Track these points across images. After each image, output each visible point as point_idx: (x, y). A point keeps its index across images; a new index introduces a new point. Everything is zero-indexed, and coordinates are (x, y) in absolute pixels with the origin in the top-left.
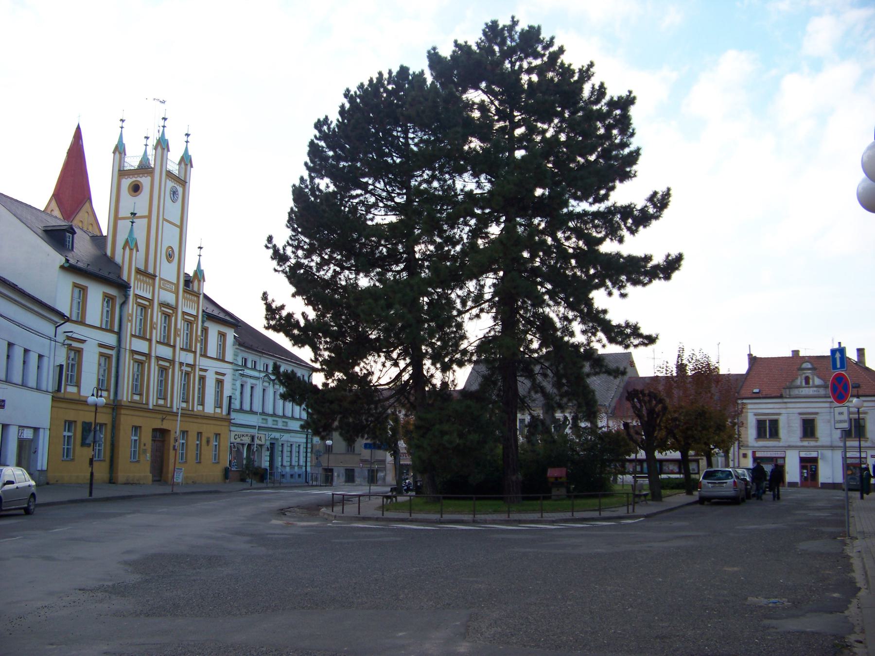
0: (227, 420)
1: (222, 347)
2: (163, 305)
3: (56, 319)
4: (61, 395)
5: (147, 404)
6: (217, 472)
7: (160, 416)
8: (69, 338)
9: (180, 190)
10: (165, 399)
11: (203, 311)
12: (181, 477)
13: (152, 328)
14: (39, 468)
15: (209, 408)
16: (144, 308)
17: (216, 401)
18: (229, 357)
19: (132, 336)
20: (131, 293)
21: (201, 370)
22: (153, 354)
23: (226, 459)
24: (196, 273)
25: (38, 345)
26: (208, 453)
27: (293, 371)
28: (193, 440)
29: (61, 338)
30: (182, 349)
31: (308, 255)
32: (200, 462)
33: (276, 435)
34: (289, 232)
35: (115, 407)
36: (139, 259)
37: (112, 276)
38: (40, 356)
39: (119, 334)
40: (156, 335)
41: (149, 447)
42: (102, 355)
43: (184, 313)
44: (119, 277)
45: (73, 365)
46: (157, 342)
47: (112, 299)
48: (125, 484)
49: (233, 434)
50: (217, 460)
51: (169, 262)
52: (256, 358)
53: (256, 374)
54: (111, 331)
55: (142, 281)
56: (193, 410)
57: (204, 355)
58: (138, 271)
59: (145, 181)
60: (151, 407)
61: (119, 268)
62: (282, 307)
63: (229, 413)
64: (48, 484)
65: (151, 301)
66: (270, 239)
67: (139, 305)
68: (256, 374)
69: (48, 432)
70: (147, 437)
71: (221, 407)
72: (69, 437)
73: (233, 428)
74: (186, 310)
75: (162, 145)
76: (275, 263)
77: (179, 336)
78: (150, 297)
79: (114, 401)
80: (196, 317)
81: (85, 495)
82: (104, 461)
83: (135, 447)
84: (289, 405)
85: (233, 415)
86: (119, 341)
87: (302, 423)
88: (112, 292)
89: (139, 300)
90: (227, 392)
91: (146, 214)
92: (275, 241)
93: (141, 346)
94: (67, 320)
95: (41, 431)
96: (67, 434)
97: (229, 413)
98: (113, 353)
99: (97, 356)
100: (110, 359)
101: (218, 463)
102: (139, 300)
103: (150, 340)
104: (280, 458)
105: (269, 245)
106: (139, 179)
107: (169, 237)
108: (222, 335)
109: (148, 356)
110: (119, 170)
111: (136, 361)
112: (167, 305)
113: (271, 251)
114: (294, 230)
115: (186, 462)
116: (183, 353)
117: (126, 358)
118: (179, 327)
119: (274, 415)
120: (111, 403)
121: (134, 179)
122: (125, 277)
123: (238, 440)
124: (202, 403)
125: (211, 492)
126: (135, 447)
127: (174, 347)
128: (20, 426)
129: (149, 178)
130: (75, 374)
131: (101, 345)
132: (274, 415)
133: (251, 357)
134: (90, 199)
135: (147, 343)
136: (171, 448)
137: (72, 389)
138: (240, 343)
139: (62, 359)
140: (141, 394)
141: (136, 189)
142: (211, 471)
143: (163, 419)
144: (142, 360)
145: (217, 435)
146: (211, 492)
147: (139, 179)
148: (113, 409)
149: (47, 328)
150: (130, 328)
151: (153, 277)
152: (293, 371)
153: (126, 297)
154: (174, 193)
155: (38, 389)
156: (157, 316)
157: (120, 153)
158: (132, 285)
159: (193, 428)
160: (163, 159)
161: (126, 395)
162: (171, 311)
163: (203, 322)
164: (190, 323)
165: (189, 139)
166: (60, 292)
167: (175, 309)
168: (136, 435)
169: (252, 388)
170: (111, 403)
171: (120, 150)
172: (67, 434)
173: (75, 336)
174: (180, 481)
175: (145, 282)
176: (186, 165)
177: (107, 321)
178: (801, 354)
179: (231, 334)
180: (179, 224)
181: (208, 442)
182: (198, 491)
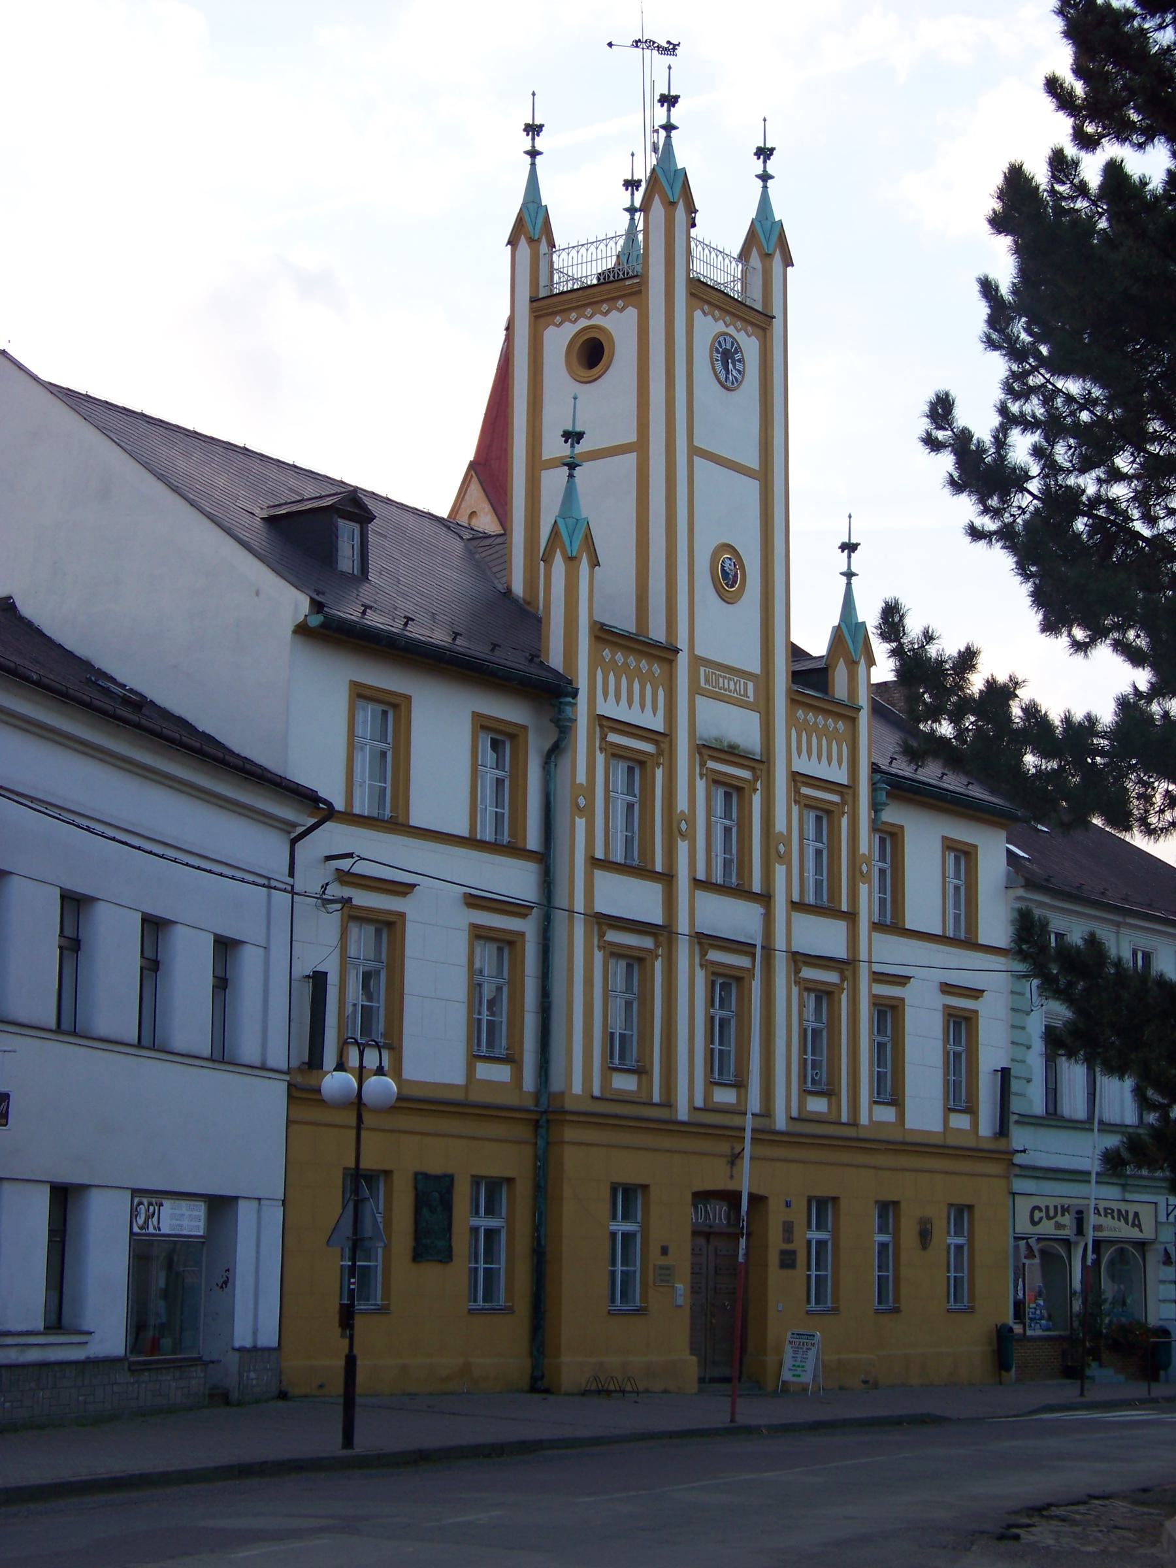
0: (999, 1155)
2: (707, 750)
3: (287, 812)
5: (668, 1103)
6: (967, 1343)
8: (344, 877)
9: (749, 346)
10: (830, 1093)
11: (875, 769)
12: (810, 1366)
13: (672, 835)
14: (242, 1337)
15: (924, 1110)
16: (637, 764)
21: (879, 977)
22: (683, 926)
25: (244, 912)
26: (924, 1276)
27: (1092, 941)
28: (860, 1233)
29: (311, 877)
30: (797, 906)
31: (1096, 450)
32: (896, 1310)
34: (998, 366)
35: (544, 1118)
36: (609, 592)
37: (510, 658)
38: (225, 947)
39: (544, 859)
41: (682, 1257)
42: (479, 934)
43: (797, 778)
44: (536, 656)
45: (723, 1023)
46: (594, 863)
47: (512, 737)
48: (584, 1393)
49: (1023, 1206)
50: (961, 1293)
51: (728, 599)
54: (514, 849)
55: (810, 730)
56: (854, 1124)
57: (891, 923)
58: (604, 635)
59: (619, 325)
60: (683, 1114)
62: (967, 659)
63: (1003, 1131)
64: (283, 1396)
66: (941, 409)
67: (616, 754)
69: (274, 1215)
70: (671, 1223)
71: (970, 1109)
72: (821, 1244)
73: (1020, 1185)
74: (803, 765)
75: (665, 191)
76: (966, 508)
77: (785, 859)
78: (657, 723)
79: (537, 1096)
80: (847, 790)
81: (329, 1442)
82: (509, 1310)
83: (490, 1254)
84: (1074, 1074)
85: (1020, 1137)
86: (547, 883)
87: (1112, 1141)
88: (508, 710)
90: (992, 1051)
91: (633, 438)
92: (963, 417)
93: (636, 899)
95: (245, 1213)
96: (621, 1227)
97: (1003, 1131)
98: (527, 927)
99: (460, 942)
100: (514, 950)
101: (971, 1310)
102: (613, 738)
103: (667, 878)
105: (941, 435)
106: (598, 320)
107: (721, 511)
109: (663, 933)
110: (534, 300)
111: (808, 987)
112: (732, 753)
113: (946, 462)
114: (1015, 353)
115: (835, 1310)
117: (576, 940)
118: (780, 825)
120: (529, 1103)
121: (583, 323)
122: (556, 660)
123: (1047, 1228)
124: (891, 1091)
125: (896, 1422)
126: (490, 1254)
127: (765, 898)
128: (135, 1192)
129: (632, 313)
130: (380, 1004)
131: (474, 901)
135: (757, 910)
136: (773, 1258)
140: (642, 1071)
142: (941, 1340)
144: (638, 951)
145: (962, 1212)
146: (896, 1422)
147: (598, 320)
148: (536, 1125)
149: (263, 849)
150: (577, 840)
152: (1092, 941)
153: (563, 728)
154: (727, 356)
155: (222, 1055)
156: (690, 791)
157: (533, 241)
158: (582, 684)
159: (858, 1187)
161: (580, 1073)
162: (746, 774)
163: (876, 807)
164: (825, 814)
166: (306, 719)
167: (761, 764)
168: (959, 1233)
170: (529, 1103)
171: (532, 229)
172: (621, 1227)
173: (361, 868)
174: (807, 1378)
175: (823, 733)
176: (767, 257)
177: (957, 917)
180: (754, 463)
181: (925, 1235)
182: (882, 1417)
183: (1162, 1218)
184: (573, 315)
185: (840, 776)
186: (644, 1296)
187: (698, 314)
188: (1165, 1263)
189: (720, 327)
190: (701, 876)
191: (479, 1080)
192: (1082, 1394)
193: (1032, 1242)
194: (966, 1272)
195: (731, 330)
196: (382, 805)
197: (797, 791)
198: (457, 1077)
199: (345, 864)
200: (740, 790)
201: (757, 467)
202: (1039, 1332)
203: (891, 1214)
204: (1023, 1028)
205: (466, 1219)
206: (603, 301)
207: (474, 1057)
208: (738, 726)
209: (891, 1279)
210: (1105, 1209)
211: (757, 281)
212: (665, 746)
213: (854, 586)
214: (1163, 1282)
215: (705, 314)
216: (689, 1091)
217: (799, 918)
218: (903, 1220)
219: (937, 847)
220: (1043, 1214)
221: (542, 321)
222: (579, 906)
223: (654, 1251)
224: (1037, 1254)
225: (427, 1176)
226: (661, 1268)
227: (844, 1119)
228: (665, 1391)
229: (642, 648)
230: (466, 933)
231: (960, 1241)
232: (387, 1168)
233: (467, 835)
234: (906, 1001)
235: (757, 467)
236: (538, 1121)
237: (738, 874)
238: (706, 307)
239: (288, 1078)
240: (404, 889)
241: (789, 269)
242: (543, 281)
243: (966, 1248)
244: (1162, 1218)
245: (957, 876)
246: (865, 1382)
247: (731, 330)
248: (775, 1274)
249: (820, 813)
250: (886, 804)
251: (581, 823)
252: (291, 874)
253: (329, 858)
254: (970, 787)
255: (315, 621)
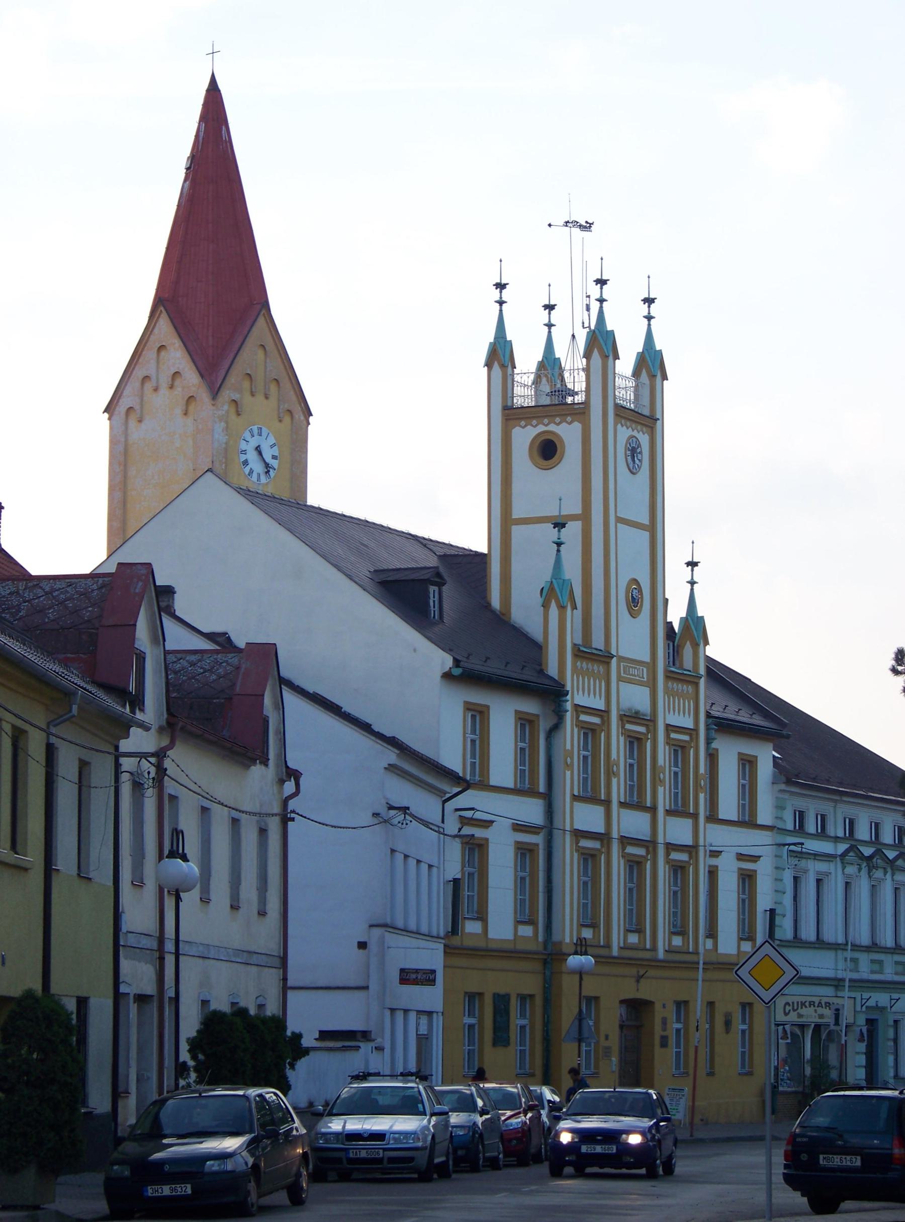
1: (748, 791)
4: (456, 941)
7: (633, 971)
9: (644, 439)
10: (640, 931)
11: (708, 715)
13: (610, 774)
15: (728, 943)
17: (741, 922)
18: (764, 816)
19: (575, 798)
20: (569, 706)
23: (768, 1058)
24: (684, 622)
26: (729, 1050)
33: (881, 998)
37: (528, 675)
39: (548, 798)
40: (618, 790)
41: (614, 1042)
43: (669, 728)
44: (541, 672)
47: (531, 722)
51: (633, 614)
52: (826, 807)
53: (826, 847)
54: (531, 792)
57: (713, 818)
60: (615, 952)
61: (537, 648)
65: (604, 714)
68: (826, 847)
75: (601, 343)
78: (600, 704)
79: (545, 943)
80: (693, 732)
86: (549, 812)
88: (530, 706)
89: (583, 717)
93: (589, 818)
94: (465, 784)
96: (468, 1020)
98: (538, 839)
101: (750, 1074)
104: (891, 1059)
106: (552, 427)
107: (630, 563)
108: (748, 764)
116: (674, 821)
118: (661, 761)
119: (874, 947)
120: (541, 948)
122: (552, 670)
123: (793, 1017)
129: (577, 426)
132: (874, 947)
133: (812, 807)
134: (266, 305)
137: (472, 927)
138: (786, 775)
139: (453, 867)
141: (548, 450)
143: (639, 978)
144: (593, 849)
147: (552, 427)
148: (545, 962)
150: (569, 781)
151: (604, 658)
153: (559, 715)
154: (633, 451)
157: (503, 366)
158: (568, 687)
160: (607, 375)
162: (642, 729)
163: (709, 741)
167: (650, 722)
169: (819, 881)
171: (500, 355)
172: (468, 1020)
173: (478, 815)
176: (652, 377)
177: (473, 765)
179: (766, 756)
181: (728, 1024)
183: (858, 1008)
185: (689, 723)
186: (597, 1066)
187: (619, 426)
188: (859, 1041)
189: (630, 432)
190: (623, 800)
191: (470, 934)
193: (787, 1027)
194: (477, 1045)
195: (635, 433)
196: (744, 815)
197: (623, 727)
198: (510, 936)
199: (468, 814)
200: (639, 740)
201: (648, 523)
202: (786, 1089)
203: (528, 1006)
204: (781, 880)
205: (516, 1021)
206: (534, 418)
208: (635, 697)
209: (476, 1051)
210: (826, 1003)
211: (646, 392)
212: (651, 728)
213: (695, 591)
214: (858, 1053)
215: (622, 426)
216: (618, 937)
217: (625, 812)
218: (717, 1014)
219: (460, 709)
220: (791, 1008)
222: (568, 828)
223: (602, 1038)
224: (789, 1036)
225: (498, 995)
227: (648, 946)
229: (593, 656)
231: (472, 1021)
232: (480, 991)
233: (736, 820)
234: (490, 841)
235: (648, 523)
236: (545, 960)
237: (638, 794)
238: (623, 421)
239: (443, 941)
240: (487, 824)
241: (665, 382)
243: (476, 1027)
244: (858, 1008)
245: (474, 732)
246: (702, 1120)
247: (635, 433)
248: (658, 1050)
249: (586, 731)
250: (715, 739)
251: (568, 773)
252: (443, 822)
253: (457, 810)
254: (754, 716)
255: (457, 672)
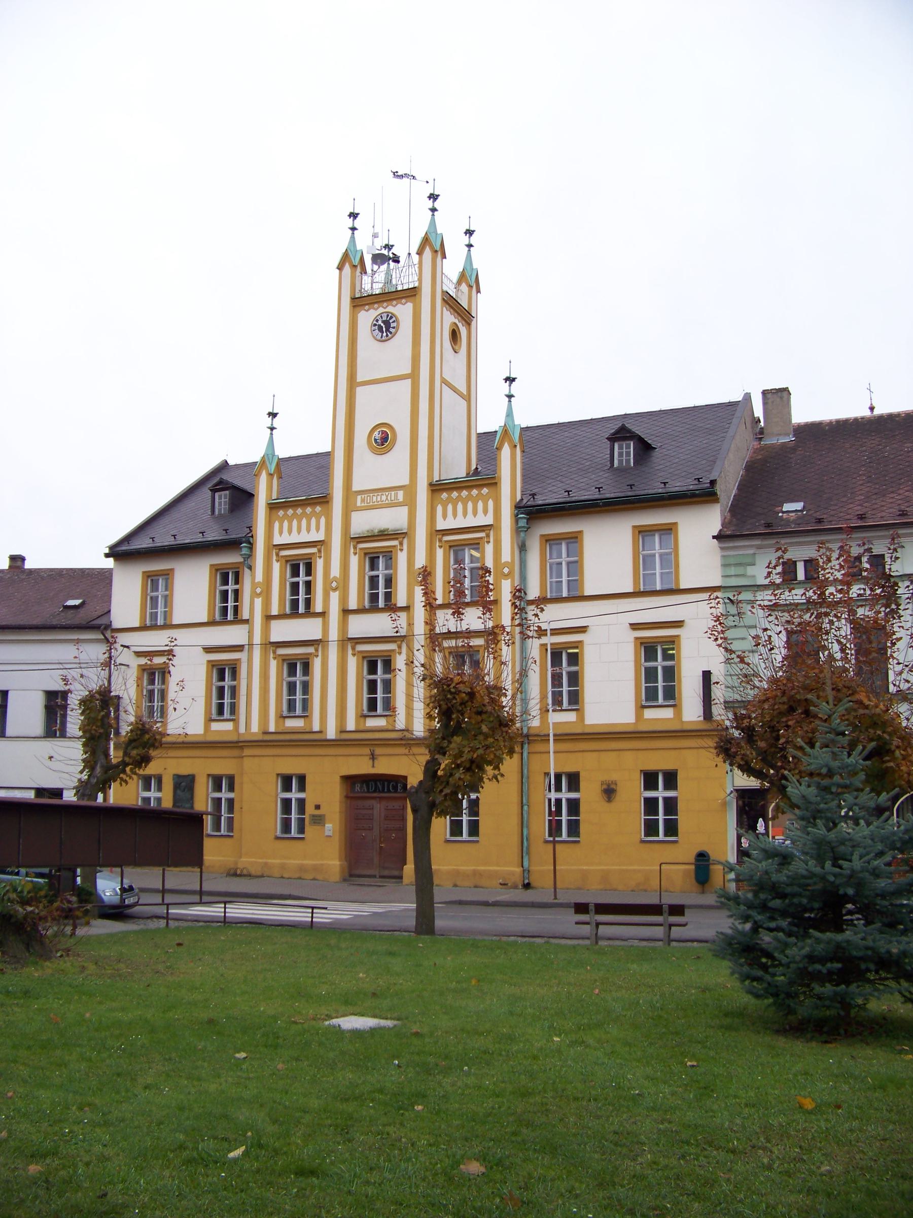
7: (367, 751)
9: (463, 330)
59: (403, 311)
96: (553, 795)
106: (390, 309)
110: (353, 299)
121: (381, 310)
129: (409, 306)
147: (390, 309)
154: (455, 335)
165: (474, 240)
178: (28, 565)
180: (464, 390)
184: (376, 306)
191: (31, 572)
192: (373, 766)
198: (201, 731)
207: (209, 720)
221: (358, 309)
226: (313, 816)
228: (314, 879)
230: (205, 666)
242: (358, 288)
